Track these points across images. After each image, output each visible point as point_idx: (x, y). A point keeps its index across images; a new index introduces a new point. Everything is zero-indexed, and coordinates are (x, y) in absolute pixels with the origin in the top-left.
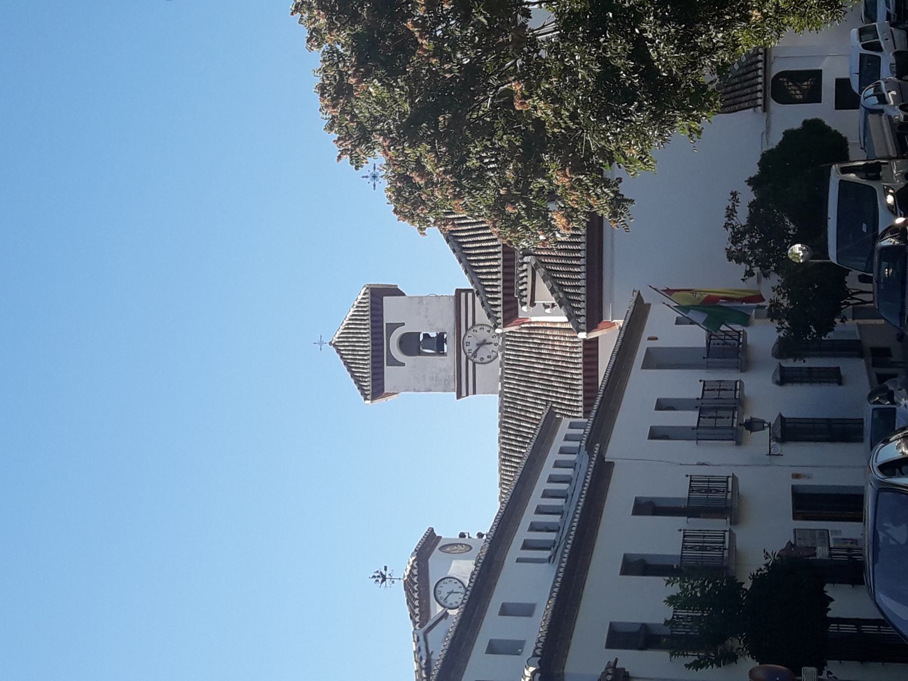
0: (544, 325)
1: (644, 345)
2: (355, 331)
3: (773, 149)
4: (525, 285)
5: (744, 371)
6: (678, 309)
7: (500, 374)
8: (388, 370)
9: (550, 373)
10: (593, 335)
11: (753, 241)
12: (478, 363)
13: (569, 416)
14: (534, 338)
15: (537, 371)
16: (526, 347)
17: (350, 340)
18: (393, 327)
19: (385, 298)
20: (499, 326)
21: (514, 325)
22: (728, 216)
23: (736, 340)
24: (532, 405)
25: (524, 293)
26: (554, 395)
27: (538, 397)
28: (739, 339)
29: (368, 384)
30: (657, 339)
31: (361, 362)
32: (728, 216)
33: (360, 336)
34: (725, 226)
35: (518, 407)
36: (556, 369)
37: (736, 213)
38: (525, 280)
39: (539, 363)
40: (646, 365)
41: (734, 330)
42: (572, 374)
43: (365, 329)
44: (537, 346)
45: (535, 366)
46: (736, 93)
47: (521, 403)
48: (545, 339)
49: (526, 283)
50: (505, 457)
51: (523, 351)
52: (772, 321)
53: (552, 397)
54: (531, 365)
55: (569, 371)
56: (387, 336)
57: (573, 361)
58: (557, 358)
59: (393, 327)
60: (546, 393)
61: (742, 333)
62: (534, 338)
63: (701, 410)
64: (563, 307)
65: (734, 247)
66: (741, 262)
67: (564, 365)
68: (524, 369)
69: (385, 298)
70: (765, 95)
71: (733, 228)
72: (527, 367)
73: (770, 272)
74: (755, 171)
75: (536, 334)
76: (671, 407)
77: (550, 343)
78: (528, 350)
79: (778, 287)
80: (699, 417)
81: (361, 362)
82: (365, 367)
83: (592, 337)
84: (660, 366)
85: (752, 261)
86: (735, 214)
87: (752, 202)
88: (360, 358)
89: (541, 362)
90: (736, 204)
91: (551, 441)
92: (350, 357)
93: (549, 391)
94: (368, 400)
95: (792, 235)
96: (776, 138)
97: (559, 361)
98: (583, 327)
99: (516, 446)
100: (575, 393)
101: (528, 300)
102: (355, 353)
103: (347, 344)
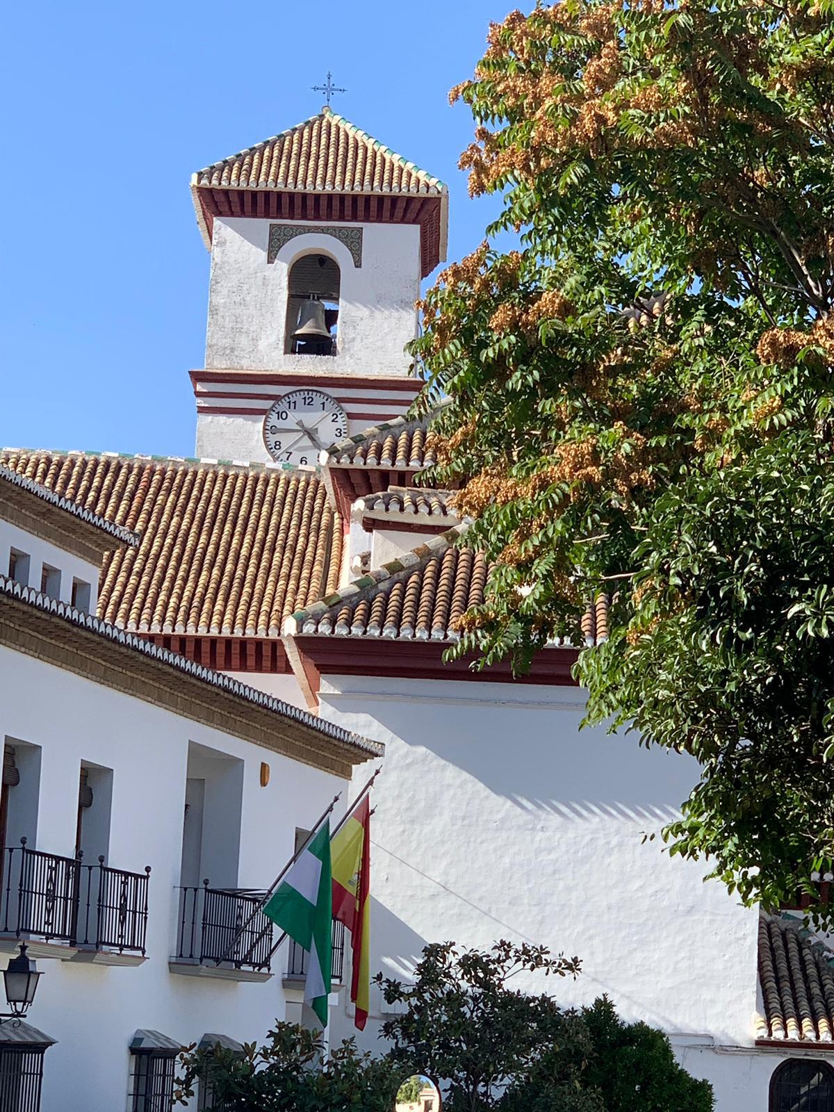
0: (334, 561)
1: (250, 753)
2: (350, 160)
3: (672, 1057)
4: (412, 508)
5: (171, 970)
6: (323, 828)
7: (235, 463)
8: (262, 225)
9: (229, 567)
10: (293, 654)
11: (466, 1003)
12: (266, 421)
13: (101, 586)
14: (307, 537)
15: (235, 541)
16: (290, 520)
17: (332, 149)
18: (354, 243)
19: (418, 227)
20: (335, 460)
21: (336, 494)
22: (526, 951)
23: (250, 952)
24: (162, 526)
25: (394, 507)
26: (181, 573)
27: (179, 540)
28: (250, 964)
29: (232, 181)
30: (264, 783)
31: (282, 169)
32: (526, 951)
33: (339, 169)
34: (503, 943)
35: (160, 497)
36: (237, 581)
37: (532, 968)
38: (423, 509)
39: (252, 547)
40: (196, 751)
41: (272, 951)
42: (223, 614)
43: (353, 181)
44: (290, 542)
45: (248, 538)
46: (800, 985)
47: (169, 504)
48: (303, 562)
49: (416, 512)
50: (52, 468)
51: (281, 515)
52: (272, 1034)
53: (177, 569)
54: (249, 530)
55: (230, 607)
56: (334, 228)
57: (251, 617)
58: (259, 583)
59: (354, 243)
60: (185, 558)
61: (264, 970)
62: (307, 537)
63: (75, 865)
64: (357, 590)
65: (455, 962)
66: (421, 973)
67: (244, 598)
68: (241, 513)
69: (418, 227)
70: (793, 1045)
71: (498, 961)
72: (247, 519)
73: (395, 1037)
74: (627, 1014)
75: (316, 543)
76: (86, 799)
77: (294, 571)
78: (283, 523)
79: (352, 1052)
80: (58, 859)
81: (282, 169)
82: (271, 178)
83: (287, 650)
84: (195, 785)
85: (420, 998)
86: (528, 965)
87: (553, 1004)
88: (292, 168)
89: (255, 549)
90: (552, 969)
91: (46, 534)
92: (295, 147)
93: (190, 563)
94: (199, 181)
95: (426, 1075)
96: (695, 1067)
97: (253, 587)
98: (309, 629)
99: (76, 488)
100: (180, 618)
101: (379, 513)
102: (302, 159)
103: (323, 141)
